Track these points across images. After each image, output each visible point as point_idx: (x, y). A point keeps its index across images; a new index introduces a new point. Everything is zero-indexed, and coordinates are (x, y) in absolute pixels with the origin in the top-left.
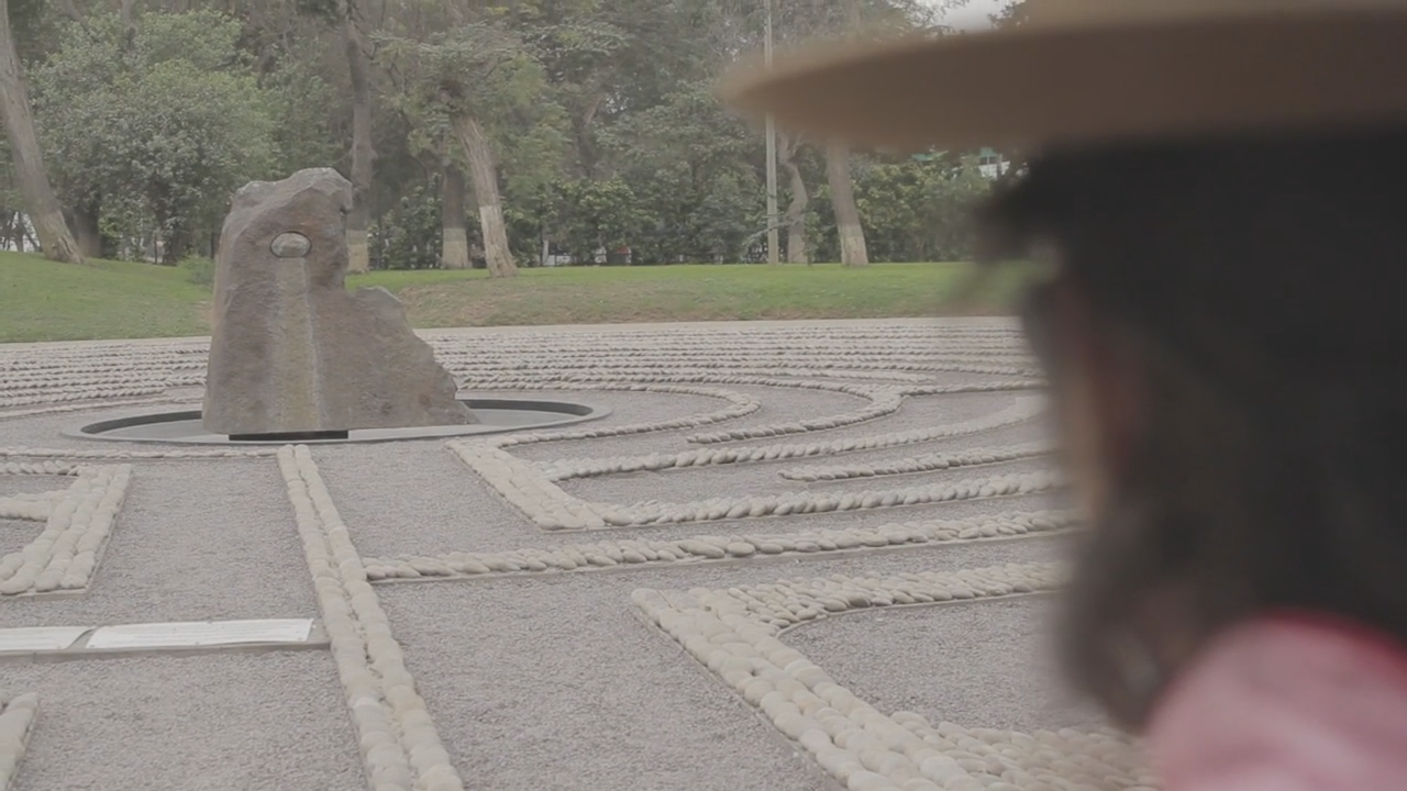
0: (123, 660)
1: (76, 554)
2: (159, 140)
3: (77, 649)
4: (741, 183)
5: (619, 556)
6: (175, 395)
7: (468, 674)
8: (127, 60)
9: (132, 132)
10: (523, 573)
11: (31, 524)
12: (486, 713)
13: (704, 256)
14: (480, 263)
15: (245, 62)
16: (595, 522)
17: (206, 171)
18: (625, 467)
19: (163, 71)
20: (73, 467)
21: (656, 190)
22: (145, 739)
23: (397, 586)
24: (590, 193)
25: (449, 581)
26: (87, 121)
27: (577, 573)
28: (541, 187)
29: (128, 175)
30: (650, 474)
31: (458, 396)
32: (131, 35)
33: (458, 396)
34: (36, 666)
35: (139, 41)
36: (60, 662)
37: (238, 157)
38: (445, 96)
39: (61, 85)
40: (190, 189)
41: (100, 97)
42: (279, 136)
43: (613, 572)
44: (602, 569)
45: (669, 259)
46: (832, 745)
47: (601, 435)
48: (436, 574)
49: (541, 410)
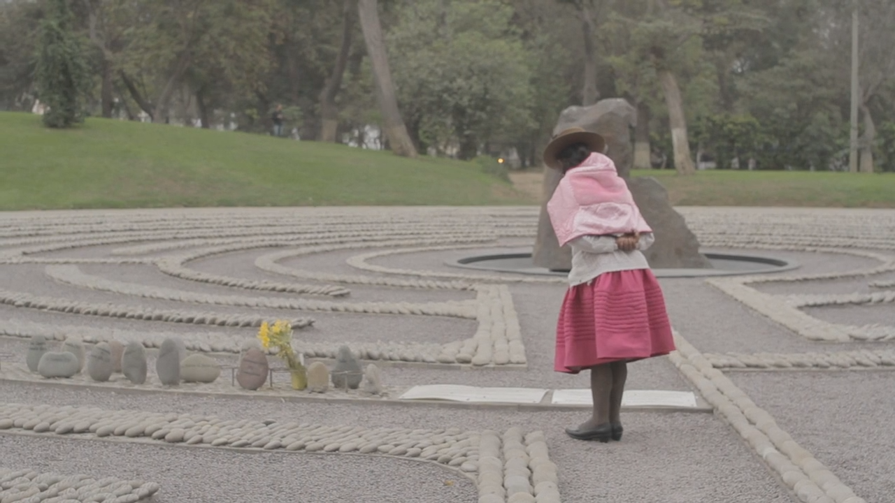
0: (577, 413)
1: (509, 341)
2: (460, 82)
3: (545, 403)
4: (831, 118)
5: (878, 360)
6: (502, 242)
7: (817, 435)
8: (441, 31)
9: (444, 77)
10: (814, 369)
11: (464, 320)
12: (844, 462)
13: (803, 165)
14: (670, 165)
15: (514, 33)
16: (843, 337)
17: (488, 102)
18: (839, 301)
19: (464, 38)
20: (470, 285)
21: (774, 122)
22: (621, 466)
23: (731, 373)
24: (731, 123)
25: (766, 372)
26: (416, 69)
27: (852, 371)
28: (699, 119)
29: (440, 103)
30: (855, 307)
31: (701, 251)
32: (443, 16)
33: (701, 251)
34: (520, 413)
35: (448, 20)
36: (536, 411)
37: (509, 94)
38: (652, 57)
39: (399, 46)
40: (478, 113)
41: (424, 53)
42: (533, 81)
43: (876, 371)
44: (868, 369)
45: (779, 166)
46: (502, 487)
47: (806, 280)
48: (757, 366)
49: (760, 262)
